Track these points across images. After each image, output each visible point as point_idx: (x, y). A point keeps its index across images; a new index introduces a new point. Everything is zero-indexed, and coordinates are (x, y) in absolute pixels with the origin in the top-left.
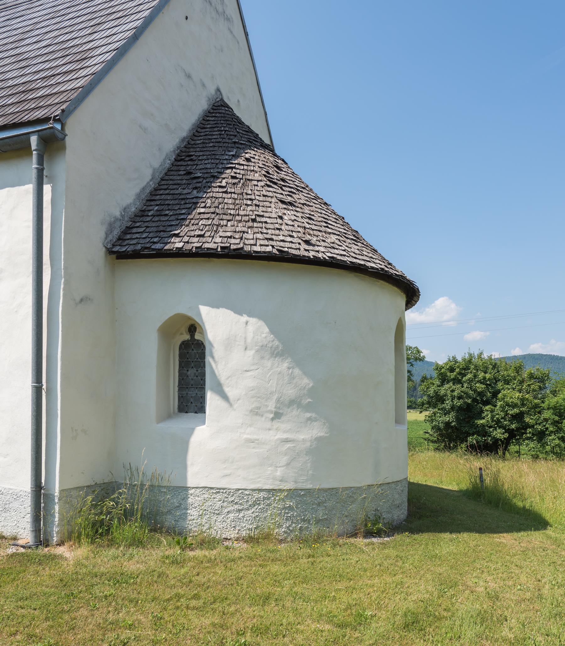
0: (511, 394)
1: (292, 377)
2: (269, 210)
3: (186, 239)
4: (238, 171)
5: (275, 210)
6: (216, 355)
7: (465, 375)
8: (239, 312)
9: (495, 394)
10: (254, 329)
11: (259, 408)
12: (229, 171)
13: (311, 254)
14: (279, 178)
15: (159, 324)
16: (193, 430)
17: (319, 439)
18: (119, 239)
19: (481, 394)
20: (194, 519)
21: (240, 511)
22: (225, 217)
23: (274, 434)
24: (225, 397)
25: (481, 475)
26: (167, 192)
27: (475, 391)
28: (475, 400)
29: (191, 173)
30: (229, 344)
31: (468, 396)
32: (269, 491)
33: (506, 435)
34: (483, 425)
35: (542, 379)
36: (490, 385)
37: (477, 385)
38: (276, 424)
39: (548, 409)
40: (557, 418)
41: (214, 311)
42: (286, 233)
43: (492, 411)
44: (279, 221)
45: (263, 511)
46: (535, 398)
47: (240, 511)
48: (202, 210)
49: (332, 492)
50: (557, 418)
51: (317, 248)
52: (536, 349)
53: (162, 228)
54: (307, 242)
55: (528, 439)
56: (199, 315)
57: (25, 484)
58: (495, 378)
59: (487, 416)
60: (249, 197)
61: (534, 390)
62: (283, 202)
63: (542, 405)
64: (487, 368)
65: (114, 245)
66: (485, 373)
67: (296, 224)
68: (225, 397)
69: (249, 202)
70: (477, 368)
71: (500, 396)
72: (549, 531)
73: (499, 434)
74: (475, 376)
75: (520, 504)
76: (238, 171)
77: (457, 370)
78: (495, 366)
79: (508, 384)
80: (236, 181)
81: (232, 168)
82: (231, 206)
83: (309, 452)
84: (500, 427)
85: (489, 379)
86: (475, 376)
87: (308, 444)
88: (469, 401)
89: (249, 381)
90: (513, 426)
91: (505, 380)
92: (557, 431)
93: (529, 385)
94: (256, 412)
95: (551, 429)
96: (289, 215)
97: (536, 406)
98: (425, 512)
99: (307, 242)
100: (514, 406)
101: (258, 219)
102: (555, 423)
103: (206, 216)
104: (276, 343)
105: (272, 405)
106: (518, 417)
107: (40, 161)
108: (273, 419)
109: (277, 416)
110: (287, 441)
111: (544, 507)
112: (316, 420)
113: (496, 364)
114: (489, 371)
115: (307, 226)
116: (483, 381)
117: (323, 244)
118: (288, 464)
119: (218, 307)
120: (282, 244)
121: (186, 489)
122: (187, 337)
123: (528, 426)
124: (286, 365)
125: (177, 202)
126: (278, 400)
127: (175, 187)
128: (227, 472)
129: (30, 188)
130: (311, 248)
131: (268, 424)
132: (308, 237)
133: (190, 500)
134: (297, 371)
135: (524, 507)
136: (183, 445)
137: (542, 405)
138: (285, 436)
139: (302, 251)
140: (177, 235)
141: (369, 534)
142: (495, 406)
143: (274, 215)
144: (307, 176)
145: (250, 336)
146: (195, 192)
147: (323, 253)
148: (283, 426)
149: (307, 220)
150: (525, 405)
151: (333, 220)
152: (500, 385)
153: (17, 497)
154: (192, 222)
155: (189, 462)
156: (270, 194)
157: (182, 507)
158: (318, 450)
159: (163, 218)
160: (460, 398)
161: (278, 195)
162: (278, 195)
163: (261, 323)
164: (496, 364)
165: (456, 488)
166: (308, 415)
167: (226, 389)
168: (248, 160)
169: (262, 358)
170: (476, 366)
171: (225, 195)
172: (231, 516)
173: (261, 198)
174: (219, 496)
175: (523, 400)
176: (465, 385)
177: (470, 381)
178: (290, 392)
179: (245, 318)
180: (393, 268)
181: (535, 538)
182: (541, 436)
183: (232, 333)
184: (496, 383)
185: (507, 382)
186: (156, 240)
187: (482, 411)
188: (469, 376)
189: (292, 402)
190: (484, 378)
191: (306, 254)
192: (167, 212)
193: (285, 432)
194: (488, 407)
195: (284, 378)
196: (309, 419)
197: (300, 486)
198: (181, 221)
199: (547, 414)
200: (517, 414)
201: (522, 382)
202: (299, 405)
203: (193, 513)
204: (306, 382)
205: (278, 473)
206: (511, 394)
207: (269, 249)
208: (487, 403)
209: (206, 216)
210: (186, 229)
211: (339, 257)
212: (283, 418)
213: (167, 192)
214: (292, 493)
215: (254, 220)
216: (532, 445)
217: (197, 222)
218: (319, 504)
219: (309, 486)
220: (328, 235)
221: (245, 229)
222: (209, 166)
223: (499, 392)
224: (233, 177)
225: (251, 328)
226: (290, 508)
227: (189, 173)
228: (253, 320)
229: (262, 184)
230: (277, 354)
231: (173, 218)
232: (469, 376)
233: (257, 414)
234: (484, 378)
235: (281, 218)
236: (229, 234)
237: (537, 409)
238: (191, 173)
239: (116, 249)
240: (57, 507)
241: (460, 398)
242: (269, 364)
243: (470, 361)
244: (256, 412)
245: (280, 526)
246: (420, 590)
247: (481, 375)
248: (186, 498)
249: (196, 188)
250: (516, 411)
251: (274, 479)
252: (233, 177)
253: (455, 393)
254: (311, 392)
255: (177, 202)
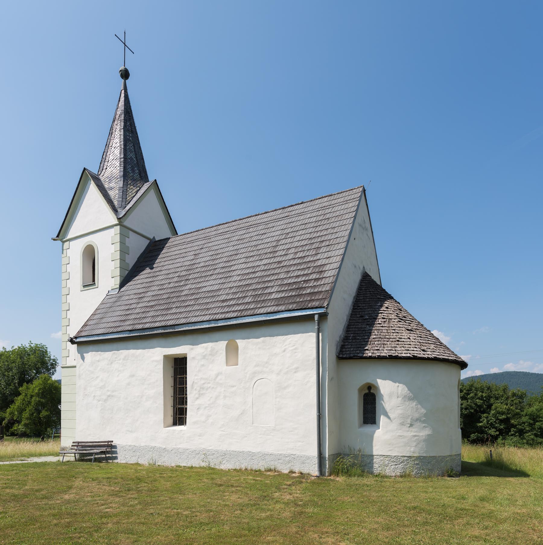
0: (499, 406)
1: (417, 409)
2: (403, 334)
3: (372, 351)
4: (385, 315)
5: (405, 334)
6: (385, 400)
7: (469, 394)
8: (395, 382)
9: (490, 406)
10: (400, 389)
11: (403, 422)
12: (380, 315)
13: (426, 356)
14: (404, 317)
15: (358, 387)
16: (375, 431)
17: (428, 435)
18: (340, 351)
19: (480, 406)
20: (377, 468)
21: (396, 465)
22: (385, 339)
23: (410, 433)
24: (389, 418)
25: (491, 454)
26: (354, 326)
27: (476, 404)
28: (475, 410)
29: (363, 316)
30: (391, 395)
31: (472, 408)
32: (408, 457)
33: (498, 433)
34: (481, 427)
35: (521, 397)
36: (485, 400)
37: (477, 400)
38: (411, 429)
39: (526, 415)
40: (532, 422)
41: (384, 382)
42: (413, 346)
43: (487, 418)
44: (408, 340)
45: (405, 465)
46: (516, 409)
47: (396, 465)
48: (375, 337)
49: (434, 457)
50: (532, 422)
51: (428, 353)
52: (510, 367)
53: (358, 346)
54: (423, 350)
55: (512, 435)
56: (377, 383)
57: (315, 453)
58: (489, 396)
59: (484, 420)
60: (393, 328)
61: (516, 404)
62: (408, 330)
63: (522, 413)
64: (483, 389)
65: (339, 354)
66: (483, 392)
67: (416, 341)
68: (389, 418)
69: (394, 331)
70: (476, 389)
71: (493, 407)
72: (531, 478)
73: (492, 432)
74: (476, 395)
75: (514, 468)
76: (385, 315)
77: (465, 391)
78: (489, 388)
79: (497, 400)
80: (385, 320)
81: (381, 313)
82: (387, 334)
83: (425, 441)
84: (493, 428)
85: (485, 397)
86: (476, 395)
87: (424, 437)
88: (472, 411)
89: (399, 411)
90: (502, 427)
91: (496, 397)
92: (531, 430)
93: (512, 401)
94: (402, 424)
95: (528, 429)
96: (412, 336)
97: (517, 414)
98: (468, 470)
99: (423, 350)
100: (503, 413)
101: (400, 340)
102: (530, 425)
103: (377, 340)
104: (411, 394)
105: (409, 421)
106: (506, 421)
107: (319, 325)
108: (409, 427)
109: (411, 425)
110: (415, 436)
111: (528, 468)
112: (427, 427)
113: (489, 387)
114: (485, 391)
115: (421, 341)
116: (481, 398)
117: (429, 350)
118: (416, 446)
119: (385, 380)
120: (413, 352)
121: (373, 456)
122: (367, 391)
123: (514, 426)
124: (415, 404)
125: (360, 332)
126: (411, 419)
127: (357, 324)
128: (391, 449)
129: (314, 335)
130: (425, 353)
131: (407, 429)
132: (423, 348)
133: (374, 460)
134: (419, 406)
135: (516, 469)
136: (371, 438)
137: (522, 413)
138: (415, 434)
139: (421, 355)
140: (367, 350)
141: (450, 476)
142: (489, 414)
143: (406, 337)
144: (419, 318)
145: (400, 392)
146: (368, 326)
147: (429, 354)
148: (414, 430)
149: (420, 338)
150: (510, 413)
151: (438, 343)
152: (492, 400)
153: (308, 458)
154: (372, 342)
155: (374, 445)
156: (401, 326)
157: (371, 463)
158: (429, 440)
159: (357, 341)
160: (466, 409)
161: (406, 326)
162: (406, 326)
163: (404, 386)
164: (489, 387)
165: (474, 462)
166: (424, 425)
167: (389, 414)
168: (387, 308)
169: (405, 401)
170: (476, 388)
171: (382, 328)
172: (393, 467)
173: (398, 329)
174: (387, 459)
175: (508, 410)
176: (469, 401)
177: (472, 398)
178: (416, 415)
179: (397, 384)
180: (460, 358)
181: (525, 480)
182: (521, 433)
183: (391, 391)
184: (489, 400)
185: (497, 399)
186: (358, 352)
187: (480, 417)
188: (472, 395)
189: (417, 420)
190: (482, 396)
191: (424, 356)
192: (358, 338)
193: (416, 432)
194: (485, 415)
195: (414, 409)
196: (424, 427)
197: (421, 455)
198: (366, 343)
199: (524, 419)
200: (504, 419)
201: (507, 398)
202: (420, 421)
203: (376, 466)
204: (423, 411)
205: (412, 450)
206: (499, 406)
207: (408, 355)
208: (484, 412)
209: (377, 340)
210: (370, 346)
211: (438, 357)
212: (414, 426)
213: (354, 326)
214: (418, 458)
215: (398, 341)
216: (515, 439)
217: (374, 342)
218: (429, 463)
219: (425, 455)
220: (429, 345)
221: (396, 345)
222: (370, 312)
223: (492, 405)
224: (383, 318)
225: (400, 389)
226: (417, 464)
227: (361, 316)
228: (401, 385)
229: (396, 320)
230: (411, 399)
231: (362, 340)
232: (472, 395)
233: (403, 425)
234: (482, 396)
235: (409, 338)
236: (390, 348)
237: (517, 415)
238: (363, 316)
239: (341, 356)
240: (327, 462)
241: (466, 409)
242: (407, 403)
243: (472, 386)
244: (402, 424)
245: (413, 471)
246: (482, 492)
247: (480, 394)
248: (373, 460)
249: (368, 325)
250: (504, 417)
251: (410, 452)
252: (383, 318)
253: (463, 406)
254: (425, 415)
255: (360, 332)
